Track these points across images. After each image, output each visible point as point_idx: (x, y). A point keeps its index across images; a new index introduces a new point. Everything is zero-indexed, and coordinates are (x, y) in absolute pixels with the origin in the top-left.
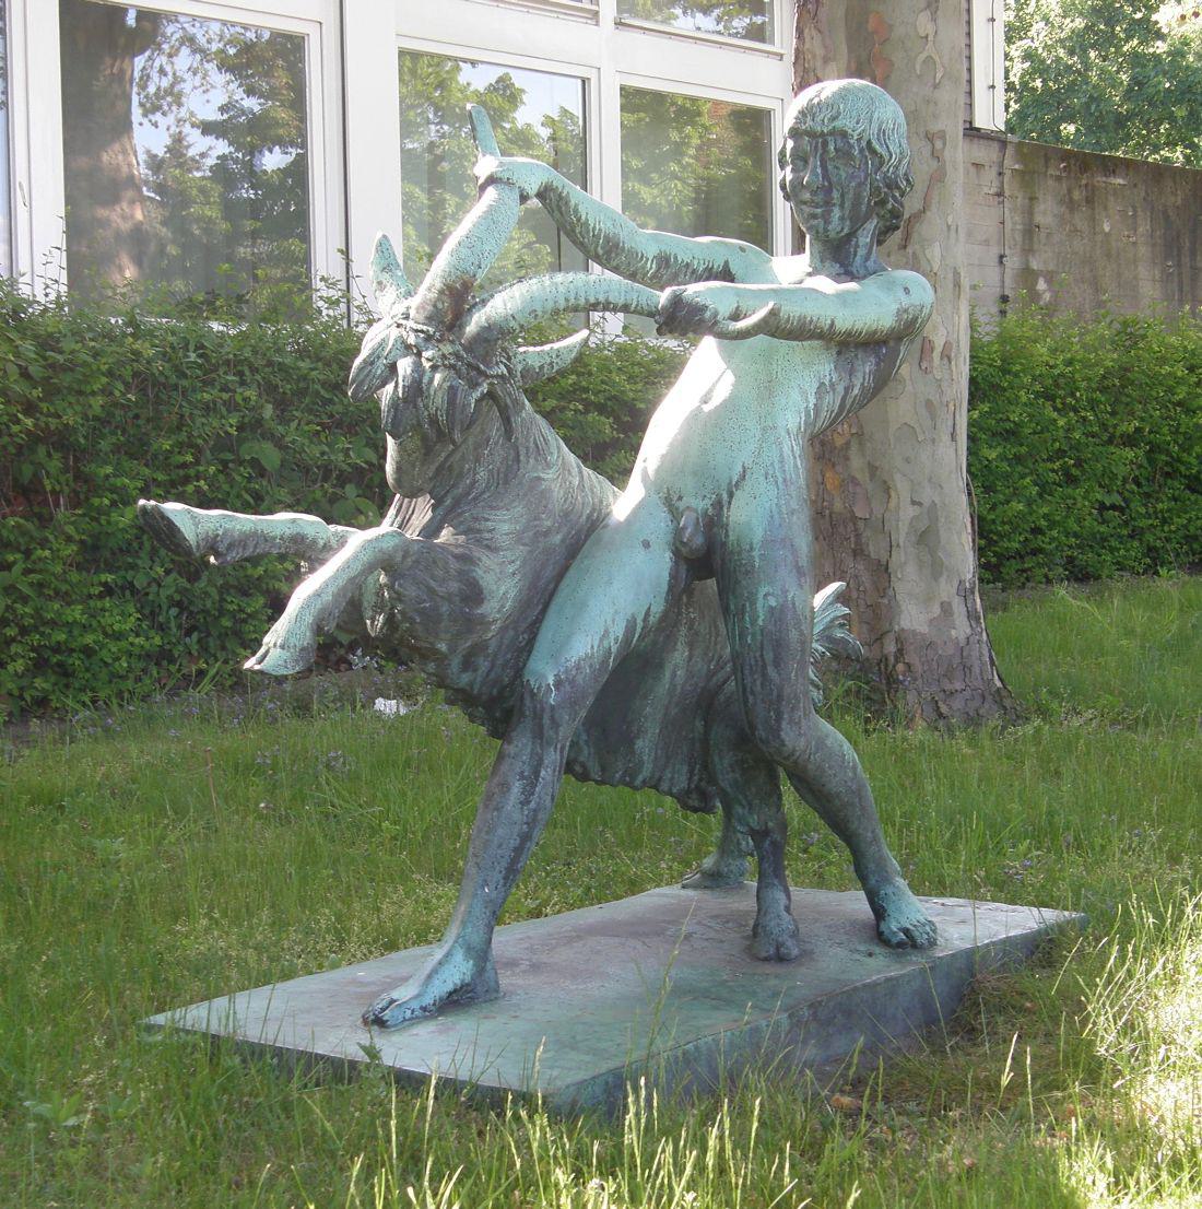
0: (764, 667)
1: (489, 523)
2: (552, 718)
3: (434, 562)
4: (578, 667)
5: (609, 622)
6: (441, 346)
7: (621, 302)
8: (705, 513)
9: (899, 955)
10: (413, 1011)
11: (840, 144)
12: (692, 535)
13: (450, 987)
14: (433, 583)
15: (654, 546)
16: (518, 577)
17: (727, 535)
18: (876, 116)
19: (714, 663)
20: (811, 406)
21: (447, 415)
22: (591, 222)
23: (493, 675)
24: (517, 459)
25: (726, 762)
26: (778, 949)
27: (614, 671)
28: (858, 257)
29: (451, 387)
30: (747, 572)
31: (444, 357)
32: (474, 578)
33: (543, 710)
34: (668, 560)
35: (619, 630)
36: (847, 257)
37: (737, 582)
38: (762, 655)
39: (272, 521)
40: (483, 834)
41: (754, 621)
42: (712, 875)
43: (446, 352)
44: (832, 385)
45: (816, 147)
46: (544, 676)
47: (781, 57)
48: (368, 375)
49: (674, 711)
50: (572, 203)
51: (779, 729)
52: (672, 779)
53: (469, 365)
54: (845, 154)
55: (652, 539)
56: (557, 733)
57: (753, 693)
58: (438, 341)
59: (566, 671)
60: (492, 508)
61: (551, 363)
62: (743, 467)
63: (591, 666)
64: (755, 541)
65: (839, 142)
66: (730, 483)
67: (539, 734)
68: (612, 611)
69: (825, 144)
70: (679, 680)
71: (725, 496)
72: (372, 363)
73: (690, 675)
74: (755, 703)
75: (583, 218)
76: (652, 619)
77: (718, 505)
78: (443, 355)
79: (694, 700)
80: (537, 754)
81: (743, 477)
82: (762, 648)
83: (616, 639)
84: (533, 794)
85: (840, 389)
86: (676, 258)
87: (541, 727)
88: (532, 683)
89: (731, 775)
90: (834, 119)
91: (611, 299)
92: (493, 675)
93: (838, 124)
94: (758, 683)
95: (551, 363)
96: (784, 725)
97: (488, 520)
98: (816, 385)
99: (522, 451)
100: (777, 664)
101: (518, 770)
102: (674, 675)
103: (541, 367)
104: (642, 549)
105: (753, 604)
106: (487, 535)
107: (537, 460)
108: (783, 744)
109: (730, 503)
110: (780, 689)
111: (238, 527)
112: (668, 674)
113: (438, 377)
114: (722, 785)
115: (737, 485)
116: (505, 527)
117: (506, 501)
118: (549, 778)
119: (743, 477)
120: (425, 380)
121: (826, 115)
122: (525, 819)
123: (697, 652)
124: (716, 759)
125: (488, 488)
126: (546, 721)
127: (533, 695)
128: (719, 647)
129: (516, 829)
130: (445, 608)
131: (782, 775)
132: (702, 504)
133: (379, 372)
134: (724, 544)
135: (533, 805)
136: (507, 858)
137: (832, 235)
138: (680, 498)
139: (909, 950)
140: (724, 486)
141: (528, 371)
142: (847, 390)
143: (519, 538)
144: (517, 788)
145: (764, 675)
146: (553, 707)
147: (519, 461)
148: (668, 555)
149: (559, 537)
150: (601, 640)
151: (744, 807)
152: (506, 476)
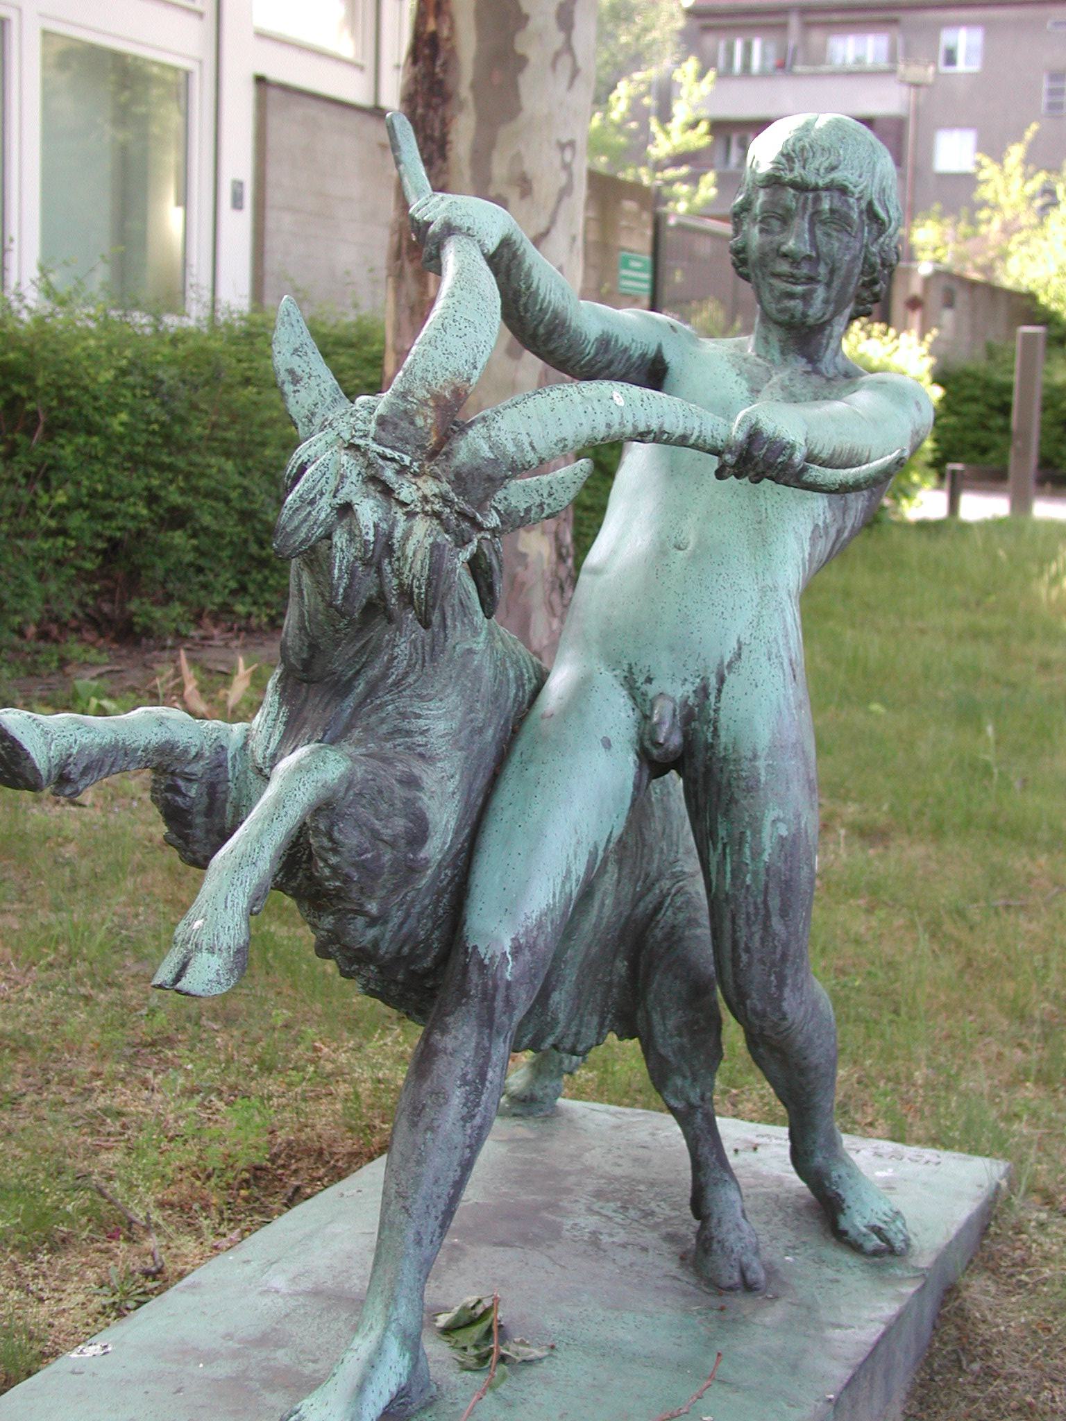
0: (767, 916)
1: (421, 722)
2: (507, 1000)
3: (380, 792)
4: (540, 926)
6: (420, 482)
7: (679, 432)
8: (685, 703)
9: (875, 1265)
11: (837, 204)
12: (670, 733)
13: (386, 1398)
15: (615, 745)
16: (457, 797)
17: (716, 733)
18: (878, 168)
19: (640, 883)
20: (807, 556)
21: (429, 584)
22: (542, 292)
23: (405, 930)
25: (671, 1023)
26: (743, 1274)
31: (425, 499)
32: (420, 809)
33: (496, 987)
34: (632, 765)
36: (817, 352)
37: (733, 800)
38: (765, 902)
39: (126, 722)
40: (412, 1164)
41: (756, 854)
42: (524, 1101)
43: (428, 493)
44: (826, 527)
45: (805, 203)
46: (498, 941)
47: (201, 15)
48: (305, 520)
49: (594, 950)
50: (526, 265)
51: (780, 998)
52: (578, 1033)
53: (462, 515)
54: (839, 219)
55: (612, 735)
58: (415, 475)
59: (526, 933)
60: (421, 698)
61: (541, 505)
62: (739, 641)
63: (552, 922)
64: (760, 748)
65: (836, 200)
66: (722, 662)
67: (488, 1023)
68: (574, 841)
69: (817, 200)
70: (607, 911)
71: (713, 681)
72: (312, 502)
73: (617, 902)
74: (750, 964)
75: (534, 286)
77: (703, 691)
79: (617, 933)
80: (484, 1049)
81: (739, 656)
82: (766, 893)
83: (577, 880)
84: (478, 1105)
86: (617, 341)
87: (491, 1010)
88: (482, 950)
89: (677, 1039)
90: (833, 168)
91: (667, 428)
92: (405, 930)
93: (835, 175)
94: (757, 937)
96: (787, 992)
97: (418, 716)
98: (810, 528)
100: (784, 913)
101: (459, 1072)
103: (528, 510)
105: (757, 832)
106: (420, 739)
108: (784, 1017)
109: (719, 691)
110: (786, 946)
111: (98, 740)
112: (596, 904)
114: (662, 1051)
115: (730, 666)
116: (441, 727)
117: (438, 686)
119: (739, 656)
120: (398, 533)
121: (821, 162)
123: (626, 871)
124: (656, 1017)
125: (411, 666)
126: (499, 1003)
127: (482, 967)
128: (645, 861)
130: (387, 857)
131: (733, 1034)
132: (682, 691)
133: (323, 515)
134: (710, 747)
135: (478, 1120)
138: (649, 680)
139: (888, 1259)
140: (713, 667)
142: (839, 532)
144: (457, 1097)
145: (766, 927)
146: (509, 985)
148: (632, 758)
150: (563, 883)
151: (685, 1077)
152: (433, 649)
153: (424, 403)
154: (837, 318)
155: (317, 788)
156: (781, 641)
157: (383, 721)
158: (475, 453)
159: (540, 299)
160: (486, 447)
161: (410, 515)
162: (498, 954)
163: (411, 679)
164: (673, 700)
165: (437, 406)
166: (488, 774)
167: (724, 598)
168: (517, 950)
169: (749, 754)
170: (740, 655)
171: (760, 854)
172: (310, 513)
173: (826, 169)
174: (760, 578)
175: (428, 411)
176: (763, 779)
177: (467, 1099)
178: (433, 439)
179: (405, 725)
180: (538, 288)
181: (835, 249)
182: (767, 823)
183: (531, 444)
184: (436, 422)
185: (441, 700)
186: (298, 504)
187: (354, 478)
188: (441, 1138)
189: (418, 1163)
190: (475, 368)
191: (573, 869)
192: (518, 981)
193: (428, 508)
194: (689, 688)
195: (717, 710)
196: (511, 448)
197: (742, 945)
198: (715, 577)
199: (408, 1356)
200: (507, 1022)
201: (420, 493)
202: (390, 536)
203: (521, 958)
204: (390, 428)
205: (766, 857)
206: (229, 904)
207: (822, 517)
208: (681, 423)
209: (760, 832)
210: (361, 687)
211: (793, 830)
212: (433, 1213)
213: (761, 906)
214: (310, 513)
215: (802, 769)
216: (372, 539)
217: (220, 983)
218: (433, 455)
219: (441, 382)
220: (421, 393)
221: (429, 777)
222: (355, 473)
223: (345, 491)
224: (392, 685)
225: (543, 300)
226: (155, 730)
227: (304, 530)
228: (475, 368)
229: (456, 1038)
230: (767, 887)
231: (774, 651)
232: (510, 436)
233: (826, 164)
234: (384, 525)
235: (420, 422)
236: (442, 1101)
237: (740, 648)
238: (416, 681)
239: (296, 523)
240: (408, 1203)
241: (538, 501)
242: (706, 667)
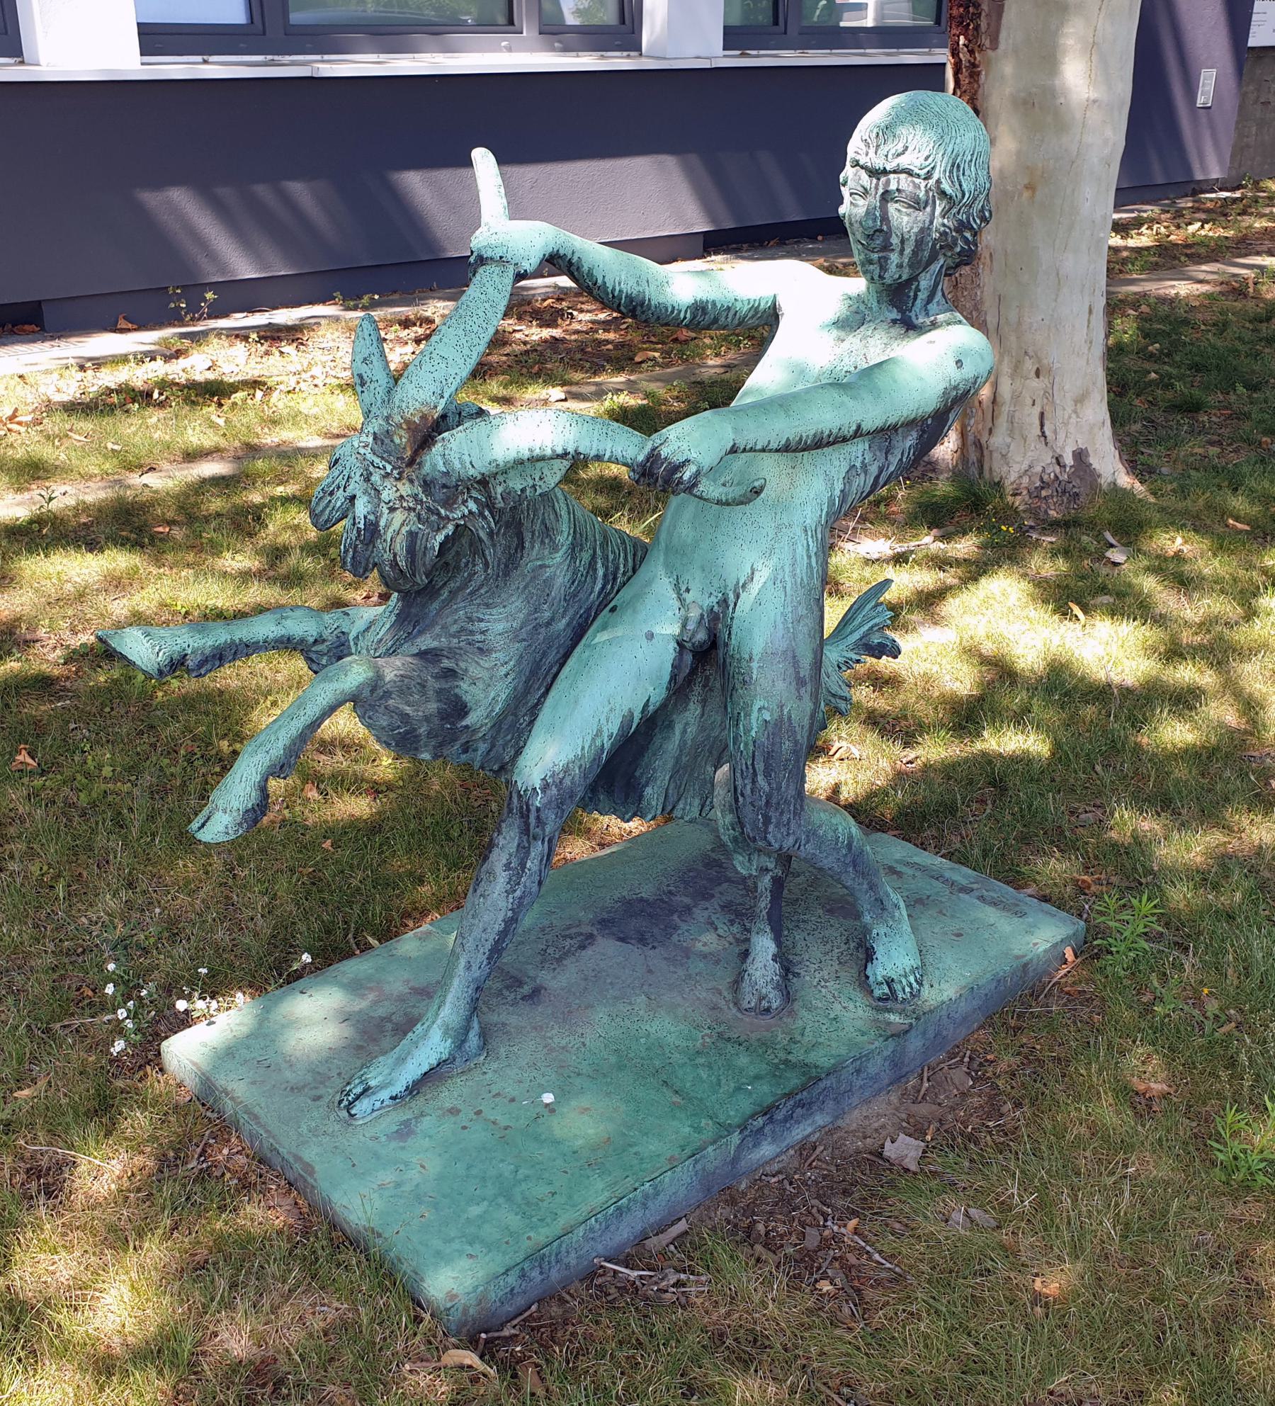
0: (755, 774)
1: (482, 625)
4: (566, 770)
5: (603, 721)
6: (399, 485)
10: (382, 1102)
14: (408, 710)
16: (510, 678)
20: (837, 492)
24: (521, 545)
27: (608, 762)
28: (918, 302)
29: (410, 533)
30: (745, 682)
32: (456, 695)
33: (528, 810)
34: (672, 651)
35: (614, 727)
38: (753, 764)
41: (747, 731)
43: (404, 494)
44: (864, 466)
48: (327, 506)
50: (585, 269)
56: (544, 830)
57: (742, 795)
58: (397, 479)
60: (488, 606)
61: (534, 486)
63: (580, 767)
64: (755, 652)
66: (738, 583)
68: (606, 709)
70: (689, 736)
72: (331, 494)
75: (600, 281)
76: (651, 708)
77: (724, 602)
78: (402, 496)
80: (524, 848)
83: (610, 736)
85: (874, 470)
87: (527, 824)
88: (519, 784)
91: (581, 450)
94: (748, 787)
95: (534, 486)
97: (481, 620)
99: (528, 536)
102: (684, 731)
103: (523, 490)
104: (644, 641)
105: (748, 715)
106: (479, 637)
107: (542, 542)
109: (735, 605)
113: (399, 517)
115: (744, 586)
116: (500, 627)
118: (535, 869)
120: (382, 523)
122: (510, 906)
126: (532, 820)
129: (501, 917)
130: (423, 730)
133: (339, 504)
136: (491, 941)
137: (888, 281)
140: (731, 586)
141: (509, 493)
143: (515, 636)
145: (754, 782)
146: (538, 810)
147: (523, 548)
149: (564, 621)
150: (593, 739)
153: (399, 426)
154: (924, 274)
155: (335, 694)
156: (787, 569)
157: (456, 621)
158: (434, 466)
159: (609, 290)
160: (441, 463)
161: (392, 510)
162: (530, 788)
163: (482, 591)
164: (701, 607)
165: (409, 429)
166: (562, 651)
167: (745, 533)
168: (546, 787)
169: (747, 657)
170: (752, 579)
171: (749, 731)
172: (330, 501)
173: (893, 155)
174: (778, 517)
175: (403, 433)
176: (754, 677)
177: (510, 879)
178: (409, 453)
179: (470, 627)
180: (605, 283)
181: (904, 224)
182: (756, 708)
183: (471, 463)
184: (409, 440)
185: (504, 607)
186: (321, 494)
187: (357, 478)
188: (489, 902)
189: (473, 917)
190: (442, 397)
191: (605, 729)
192: (545, 806)
193: (405, 504)
194: (714, 600)
195: (732, 619)
196: (457, 465)
197: (739, 791)
198: (741, 515)
199: (450, 1041)
200: (541, 832)
201: (398, 494)
202: (376, 524)
203: (548, 792)
204: (379, 443)
205: (753, 734)
206: (244, 779)
207: (860, 459)
208: (594, 446)
209: (750, 715)
210: (445, 594)
211: (775, 716)
212: (482, 951)
213: (750, 767)
214: (330, 501)
215: (791, 670)
216: (363, 527)
217: (227, 833)
218: (411, 463)
219: (411, 411)
220: (397, 419)
221: (476, 668)
222: (358, 474)
223: (351, 487)
224: (469, 594)
225: (614, 290)
226: (272, 629)
227: (327, 512)
228: (442, 397)
229: (505, 838)
230: (754, 752)
231: (780, 577)
232: (457, 456)
233: (893, 151)
234: (372, 517)
235: (397, 440)
236: (492, 879)
237: (753, 573)
238: (486, 592)
239: (320, 508)
240: (464, 941)
241: (531, 483)
242: (726, 586)
